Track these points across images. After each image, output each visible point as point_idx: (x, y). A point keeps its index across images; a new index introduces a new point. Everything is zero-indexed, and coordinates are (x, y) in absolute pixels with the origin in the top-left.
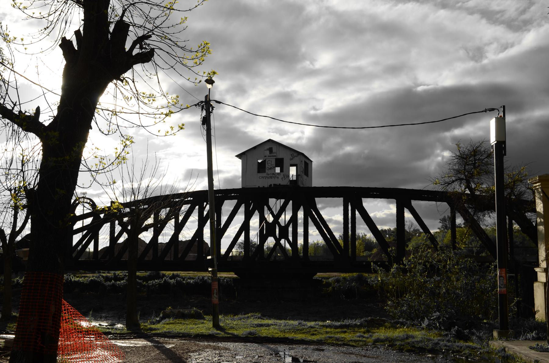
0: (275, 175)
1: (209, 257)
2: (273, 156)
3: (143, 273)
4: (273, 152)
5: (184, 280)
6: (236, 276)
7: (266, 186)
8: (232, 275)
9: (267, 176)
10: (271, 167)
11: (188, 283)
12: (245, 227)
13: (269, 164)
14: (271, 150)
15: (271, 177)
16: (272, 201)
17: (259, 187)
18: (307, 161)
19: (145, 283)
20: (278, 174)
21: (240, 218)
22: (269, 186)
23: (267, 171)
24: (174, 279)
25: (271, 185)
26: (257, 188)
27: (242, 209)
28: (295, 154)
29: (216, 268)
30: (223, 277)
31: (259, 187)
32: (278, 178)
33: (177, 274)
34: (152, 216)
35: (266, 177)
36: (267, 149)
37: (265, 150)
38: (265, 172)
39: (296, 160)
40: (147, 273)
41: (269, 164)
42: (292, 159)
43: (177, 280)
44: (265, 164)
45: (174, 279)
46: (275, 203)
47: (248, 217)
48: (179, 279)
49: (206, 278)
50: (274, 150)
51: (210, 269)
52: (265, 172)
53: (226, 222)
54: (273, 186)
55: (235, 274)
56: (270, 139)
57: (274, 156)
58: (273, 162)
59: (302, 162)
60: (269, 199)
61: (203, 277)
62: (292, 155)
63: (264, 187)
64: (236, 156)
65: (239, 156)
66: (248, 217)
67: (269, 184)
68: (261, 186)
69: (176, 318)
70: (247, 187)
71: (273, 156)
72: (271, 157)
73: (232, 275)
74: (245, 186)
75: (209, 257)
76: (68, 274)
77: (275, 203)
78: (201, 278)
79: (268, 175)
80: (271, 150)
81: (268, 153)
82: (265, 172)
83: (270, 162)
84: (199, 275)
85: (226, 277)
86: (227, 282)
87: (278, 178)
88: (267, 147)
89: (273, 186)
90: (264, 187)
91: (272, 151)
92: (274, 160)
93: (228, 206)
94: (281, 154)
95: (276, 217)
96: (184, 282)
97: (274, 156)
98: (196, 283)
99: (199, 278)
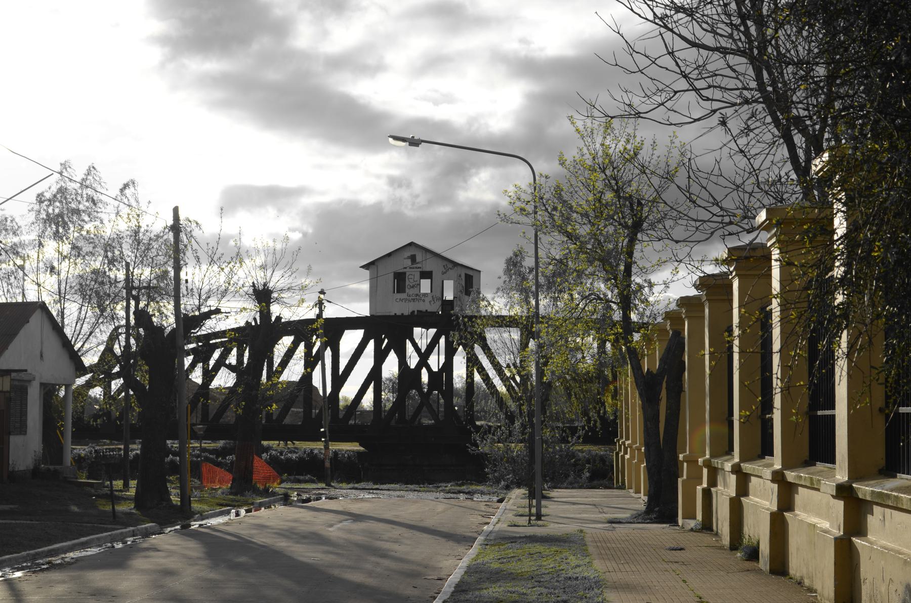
0: (419, 297)
1: (322, 430)
2: (416, 268)
3: (210, 443)
4: (417, 261)
5: (281, 454)
6: (362, 449)
7: (406, 313)
8: (355, 447)
9: (408, 298)
10: (414, 284)
11: (289, 460)
12: (375, 375)
13: (412, 281)
14: (413, 258)
15: (414, 300)
16: (417, 331)
17: (395, 314)
18: (470, 273)
19: (220, 459)
20: (425, 295)
21: (366, 363)
22: (411, 313)
23: (407, 290)
24: (267, 453)
25: (413, 312)
26: (392, 316)
27: (371, 345)
28: (450, 266)
29: (328, 438)
30: (343, 450)
31: (395, 314)
32: (424, 301)
33: (269, 445)
34: (232, 353)
35: (406, 300)
36: (408, 258)
37: (405, 259)
38: (404, 291)
39: (453, 272)
40: (220, 444)
41: (412, 281)
42: (445, 273)
43: (270, 454)
44: (405, 280)
45: (267, 453)
46: (422, 336)
47: (380, 357)
48: (274, 452)
49: (316, 452)
50: (418, 259)
51: (323, 439)
52: (405, 292)
53: (347, 367)
54: (416, 313)
55: (361, 445)
56: (412, 242)
57: (419, 268)
58: (418, 275)
59: (460, 276)
60: (414, 328)
61: (312, 450)
62: (446, 267)
63: (402, 314)
64: (362, 267)
65: (366, 267)
66: (380, 357)
67: (411, 311)
68: (399, 313)
69: (292, 483)
70: (378, 314)
71: (416, 268)
72: (413, 270)
73: (355, 447)
74: (374, 314)
75: (322, 430)
76: (90, 444)
77: (422, 336)
78: (308, 451)
79: (410, 296)
80: (413, 258)
81: (409, 262)
82: (405, 292)
83: (412, 277)
84: (304, 447)
85: (347, 450)
86: (349, 457)
87: (424, 301)
88: (408, 253)
89: (416, 313)
90: (402, 314)
91: (416, 260)
92: (419, 273)
93: (350, 339)
94: (429, 265)
95: (424, 357)
96: (283, 457)
97: (419, 268)
98: (301, 459)
99: (305, 452)
